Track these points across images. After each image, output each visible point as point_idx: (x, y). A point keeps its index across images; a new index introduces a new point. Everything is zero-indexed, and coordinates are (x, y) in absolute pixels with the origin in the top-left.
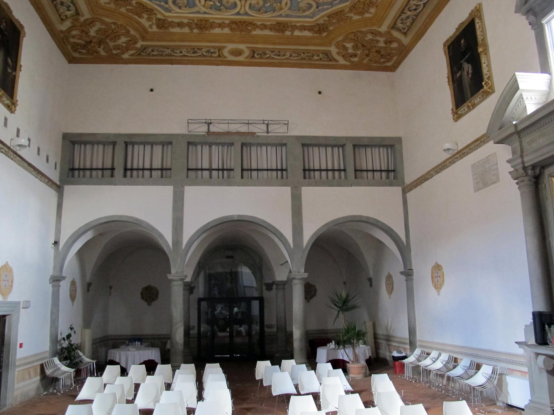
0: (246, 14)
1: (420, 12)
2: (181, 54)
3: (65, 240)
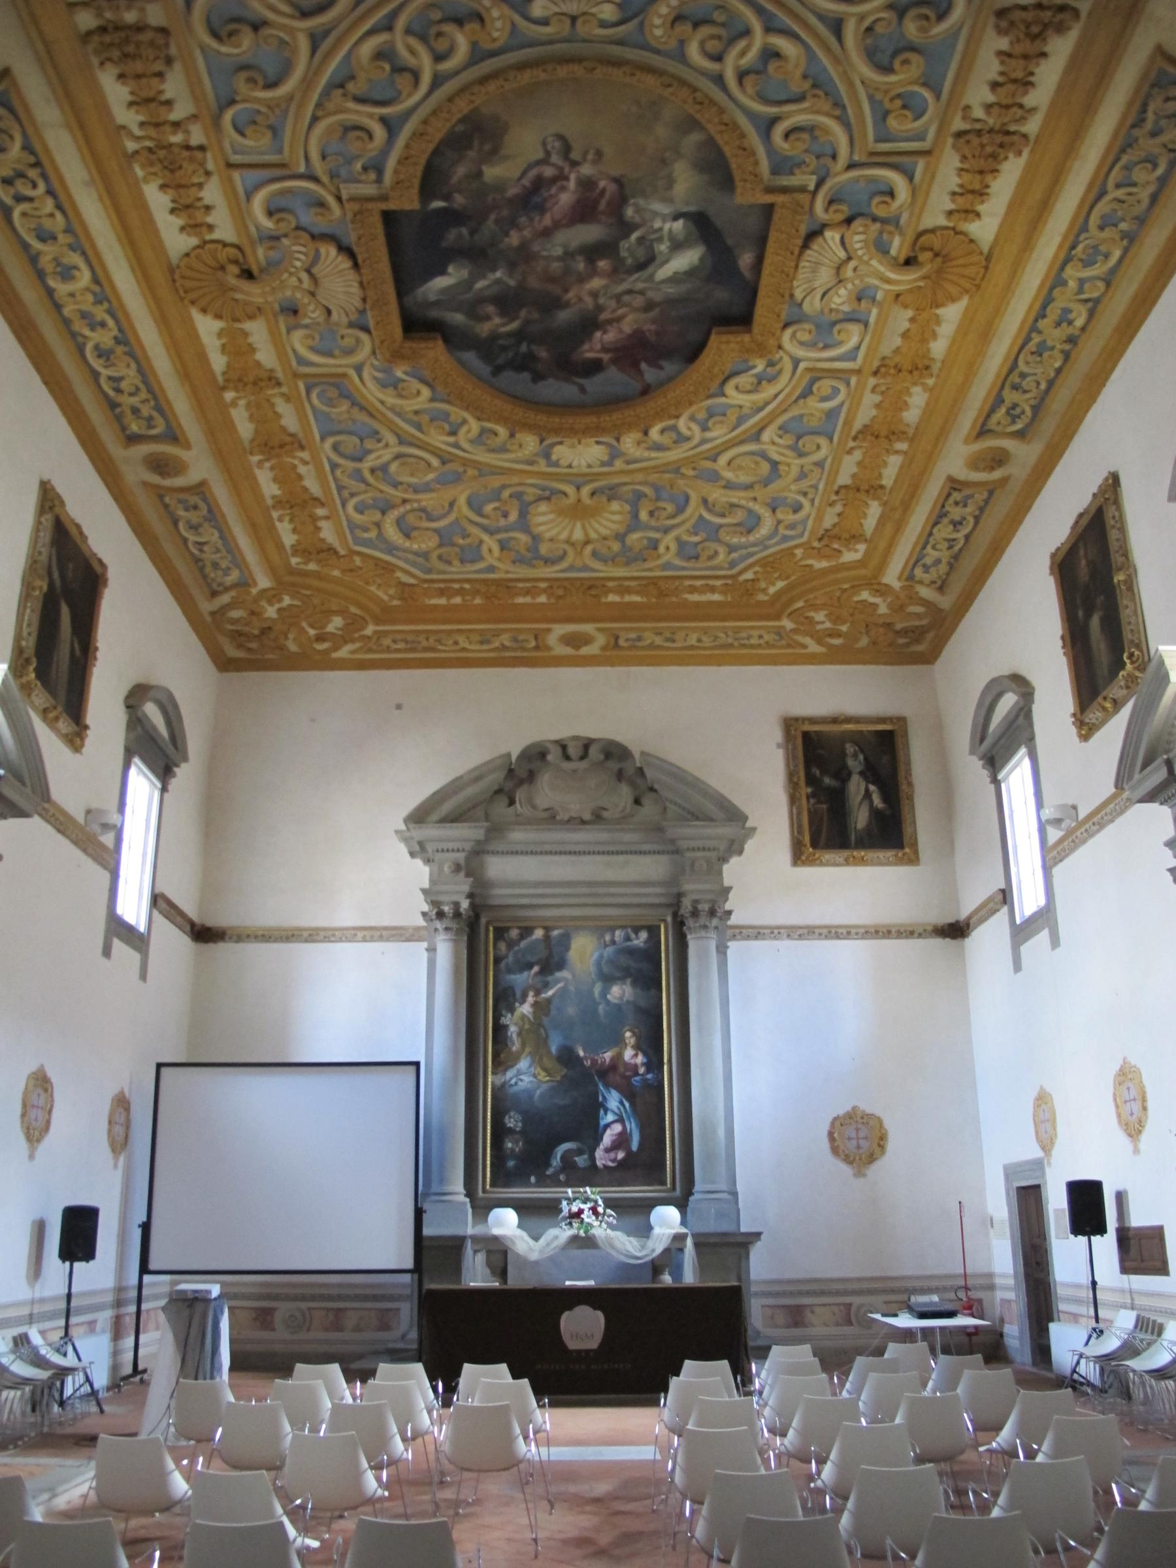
0: (586, 568)
1: (961, 550)
2: (458, 647)
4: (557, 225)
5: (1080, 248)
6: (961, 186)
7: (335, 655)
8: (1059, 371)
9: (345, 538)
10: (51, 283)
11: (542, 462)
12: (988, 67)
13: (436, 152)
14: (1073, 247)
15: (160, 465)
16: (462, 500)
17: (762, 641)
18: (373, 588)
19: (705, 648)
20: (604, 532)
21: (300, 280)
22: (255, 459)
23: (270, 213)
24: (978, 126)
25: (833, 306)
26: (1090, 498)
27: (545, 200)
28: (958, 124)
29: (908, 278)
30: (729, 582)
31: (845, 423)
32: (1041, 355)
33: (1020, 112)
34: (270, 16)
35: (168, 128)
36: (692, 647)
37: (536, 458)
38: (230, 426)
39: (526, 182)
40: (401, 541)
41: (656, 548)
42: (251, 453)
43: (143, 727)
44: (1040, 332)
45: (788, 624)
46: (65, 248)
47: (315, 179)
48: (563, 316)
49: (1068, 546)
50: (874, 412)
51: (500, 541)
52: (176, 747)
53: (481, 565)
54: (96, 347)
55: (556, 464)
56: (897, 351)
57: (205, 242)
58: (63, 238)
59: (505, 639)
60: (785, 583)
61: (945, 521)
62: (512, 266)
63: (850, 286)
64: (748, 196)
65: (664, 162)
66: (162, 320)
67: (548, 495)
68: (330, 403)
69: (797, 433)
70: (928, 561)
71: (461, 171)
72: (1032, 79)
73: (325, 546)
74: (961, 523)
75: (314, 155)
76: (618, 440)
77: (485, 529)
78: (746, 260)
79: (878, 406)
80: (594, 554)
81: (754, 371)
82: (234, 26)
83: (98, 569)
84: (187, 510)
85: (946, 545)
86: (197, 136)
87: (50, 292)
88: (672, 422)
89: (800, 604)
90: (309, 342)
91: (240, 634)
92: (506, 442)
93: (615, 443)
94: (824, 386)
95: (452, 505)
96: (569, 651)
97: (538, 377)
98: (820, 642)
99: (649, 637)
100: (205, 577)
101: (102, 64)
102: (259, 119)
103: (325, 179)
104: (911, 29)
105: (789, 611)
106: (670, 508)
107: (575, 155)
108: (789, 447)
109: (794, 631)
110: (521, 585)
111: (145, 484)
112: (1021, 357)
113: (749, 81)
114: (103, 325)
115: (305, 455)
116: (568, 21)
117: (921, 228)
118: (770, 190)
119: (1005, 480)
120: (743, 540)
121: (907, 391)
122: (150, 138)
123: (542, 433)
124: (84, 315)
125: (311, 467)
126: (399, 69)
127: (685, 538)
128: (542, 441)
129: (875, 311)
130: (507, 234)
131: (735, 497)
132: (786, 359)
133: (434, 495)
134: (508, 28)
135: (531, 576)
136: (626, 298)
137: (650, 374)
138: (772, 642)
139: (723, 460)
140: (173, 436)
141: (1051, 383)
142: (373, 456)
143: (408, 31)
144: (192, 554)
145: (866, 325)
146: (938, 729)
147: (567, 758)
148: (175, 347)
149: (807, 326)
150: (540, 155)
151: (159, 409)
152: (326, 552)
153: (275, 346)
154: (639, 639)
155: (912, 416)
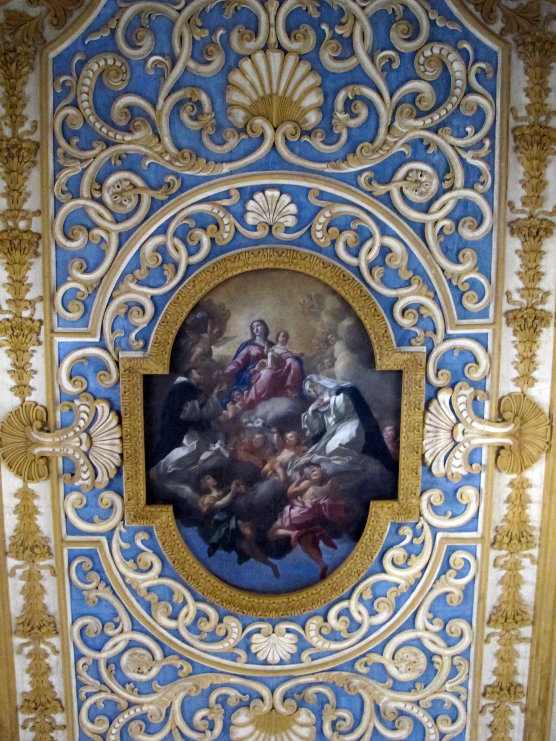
4: (259, 399)
12: (514, 263)
22: (18, 641)
24: (518, 307)
27: (251, 375)
28: (506, 307)
31: (480, 598)
34: (99, 221)
37: (237, 651)
39: (239, 360)
47: (105, 348)
56: (506, 519)
65: (328, 344)
67: (249, 699)
69: (442, 610)
71: (198, 350)
75: (107, 329)
76: (304, 628)
78: (388, 432)
97: (243, 558)
103: (111, 348)
107: (271, 337)
108: (437, 633)
113: (377, 271)
115: (55, 641)
130: (225, 408)
132: (427, 528)
133: (154, 697)
136: (307, 470)
137: (327, 554)
150: (249, 337)
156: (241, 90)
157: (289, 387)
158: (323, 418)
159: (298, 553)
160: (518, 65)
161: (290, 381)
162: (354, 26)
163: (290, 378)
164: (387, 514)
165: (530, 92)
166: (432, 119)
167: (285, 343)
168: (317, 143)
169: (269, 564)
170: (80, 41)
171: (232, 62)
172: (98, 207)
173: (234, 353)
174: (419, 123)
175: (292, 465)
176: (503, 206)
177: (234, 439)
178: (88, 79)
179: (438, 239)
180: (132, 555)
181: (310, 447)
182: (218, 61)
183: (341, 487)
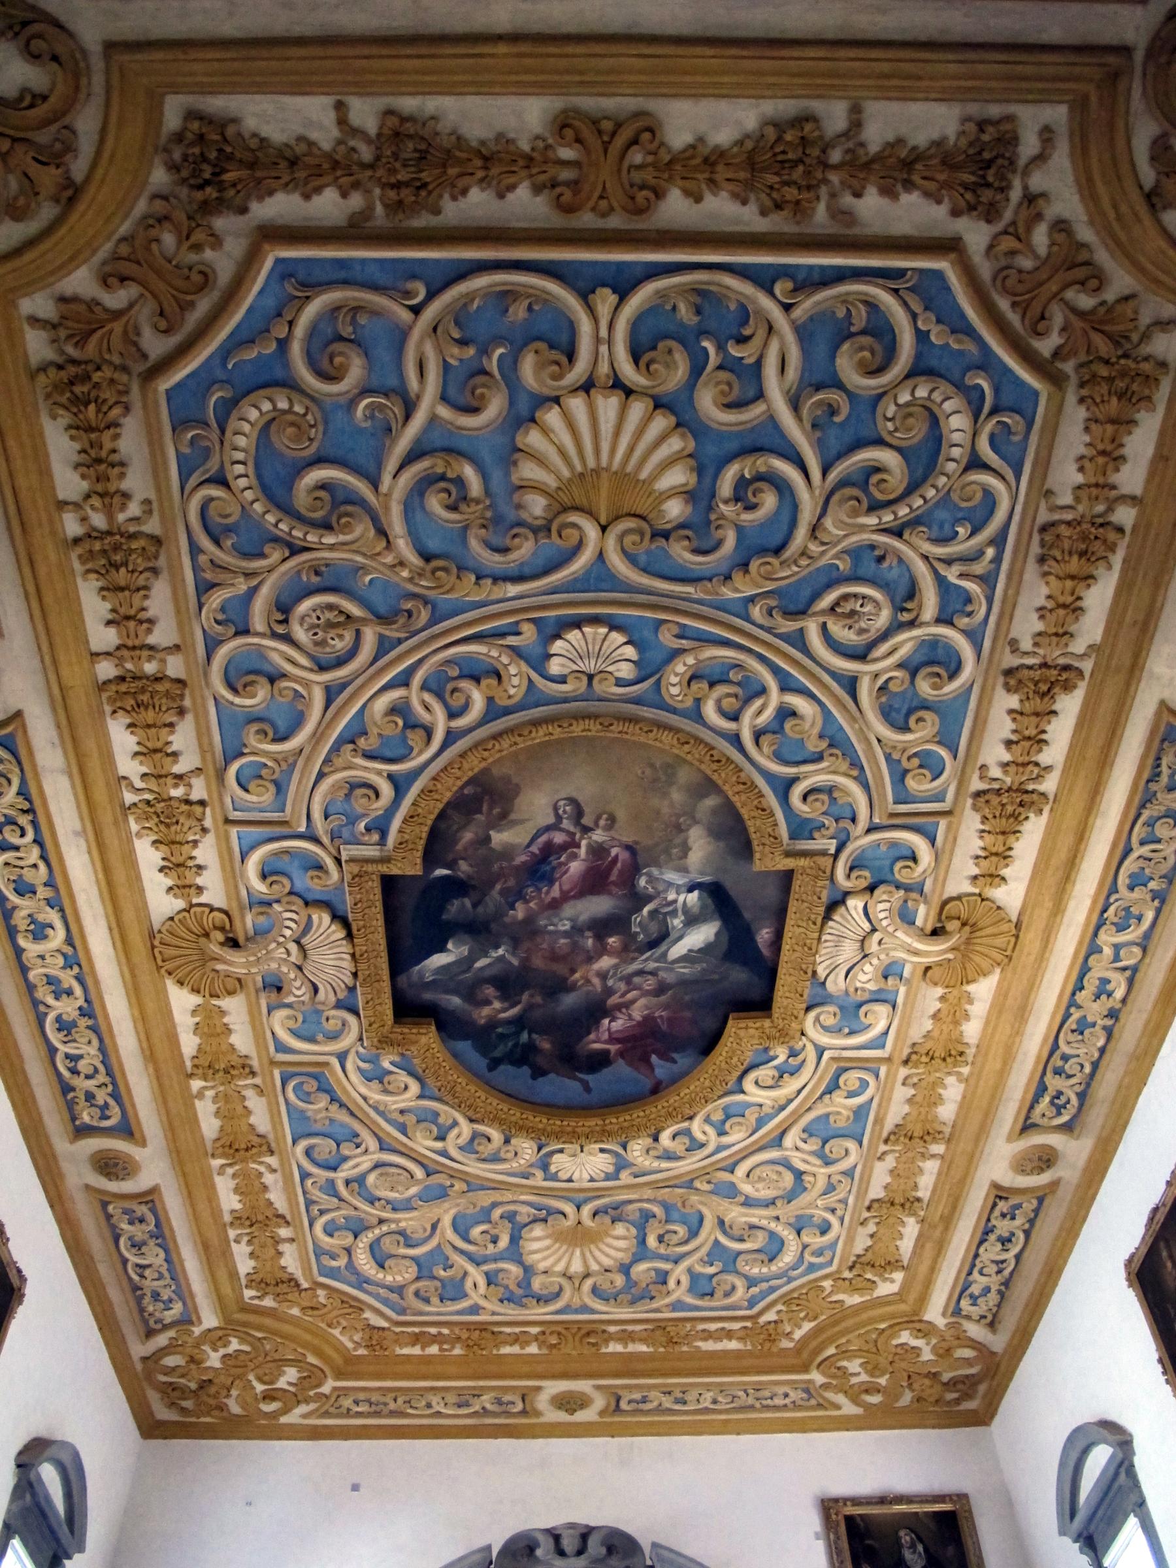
0: (585, 1309)
1: (1012, 1273)
3: (1097, 1473)
4: (565, 897)
5: (1112, 910)
6: (984, 849)
7: (284, 1420)
8: (1102, 1051)
9: (310, 1269)
10: (22, 942)
11: (539, 1174)
12: (1001, 726)
13: (442, 816)
14: (1105, 911)
15: (108, 1165)
16: (447, 1220)
17: (787, 1401)
18: (336, 1332)
19: (720, 1412)
20: (607, 1262)
21: (288, 953)
22: (217, 1163)
23: (264, 877)
24: (996, 786)
25: (859, 985)
26: (1163, 1187)
27: (554, 869)
28: (976, 785)
29: (935, 950)
30: (749, 1324)
31: (876, 1121)
32: (1082, 1033)
33: (1036, 771)
34: (289, 668)
35: (170, 781)
36: (706, 1410)
37: (533, 1171)
38: (194, 1121)
39: (534, 849)
40: (373, 1272)
41: (665, 1283)
42: (213, 1156)
43: (34, 1495)
44: (1079, 1007)
45: (817, 1377)
46: (43, 903)
47: (316, 840)
48: (569, 1001)
49: (1144, 1250)
50: (907, 1109)
51: (487, 1274)
52: (72, 1532)
53: (464, 1304)
54: (58, 1019)
55: (554, 1177)
56: (928, 1035)
57: (192, 906)
58: (43, 892)
59: (486, 1400)
60: (813, 1324)
61: (992, 1237)
62: (516, 943)
63: (875, 961)
64: (767, 861)
65: (679, 829)
66: (134, 991)
67: (545, 1216)
68: (306, 1098)
69: (823, 1134)
70: (975, 1289)
71: (468, 836)
72: (1044, 736)
73: (285, 1277)
74: (1010, 1241)
75: (317, 815)
77: (470, 1257)
78: (764, 936)
79: (910, 1101)
80: (595, 1291)
81: (775, 1063)
82: (252, 677)
83: (15, 1281)
84: (131, 1223)
85: (995, 1268)
86: (199, 791)
87: (19, 952)
88: (685, 1124)
89: (831, 1351)
90: (291, 1024)
91: (174, 1387)
92: (499, 1150)
93: (621, 1151)
94: (851, 1079)
95: (434, 1227)
96: (562, 1416)
97: (538, 1073)
98: (855, 1401)
99: (656, 1398)
100: (142, 1310)
101: (114, 712)
102: (264, 772)
103: (326, 840)
104: (924, 687)
105: (819, 1359)
106: (682, 1231)
107: (587, 821)
108: (813, 1153)
109: (825, 1386)
110: (508, 1330)
111: (87, 1187)
112: (1062, 1035)
113: (765, 741)
114: (69, 993)
115: (272, 1161)
116: (585, 679)
117: (946, 896)
118: (788, 854)
119: (1055, 1185)
120: (765, 1270)
121: (940, 1083)
122: (151, 791)
123: (541, 1137)
124: (51, 981)
125: (278, 1175)
126: (412, 725)
127: (699, 1269)
128: (539, 1149)
129: (902, 990)
130: (512, 907)
131: (757, 1216)
132: (810, 1047)
133: (415, 1214)
134: (525, 682)
135: (521, 1318)
137: (661, 1068)
138: (800, 1402)
139: (741, 1170)
140: (128, 1130)
141: (1095, 1065)
142: (351, 1163)
143: (424, 687)
144: (130, 1279)
145: (894, 1007)
146: (1009, 1506)
147: (561, 1553)
148: (142, 1019)
149: (831, 1009)
150: (551, 820)
151: (116, 1096)
152: (284, 1284)
153: (254, 1028)
154: (644, 1400)
155: (947, 1112)
156: (540, 460)
157: (613, 883)
158: (665, 920)
159: (621, 1068)
160: (1076, 414)
161: (617, 875)
162: (765, 345)
163: (615, 872)
164: (752, 1037)
165: (1087, 464)
166: (895, 513)
167: (609, 827)
168: (680, 552)
169: (576, 1079)
170: (217, 361)
171: (523, 407)
172: (284, 647)
173: (527, 841)
174: (872, 520)
175: (615, 974)
176: (1000, 642)
177: (526, 945)
178: (244, 436)
179: (878, 698)
180: (378, 1077)
181: (642, 954)
182: (495, 407)
183: (687, 998)
